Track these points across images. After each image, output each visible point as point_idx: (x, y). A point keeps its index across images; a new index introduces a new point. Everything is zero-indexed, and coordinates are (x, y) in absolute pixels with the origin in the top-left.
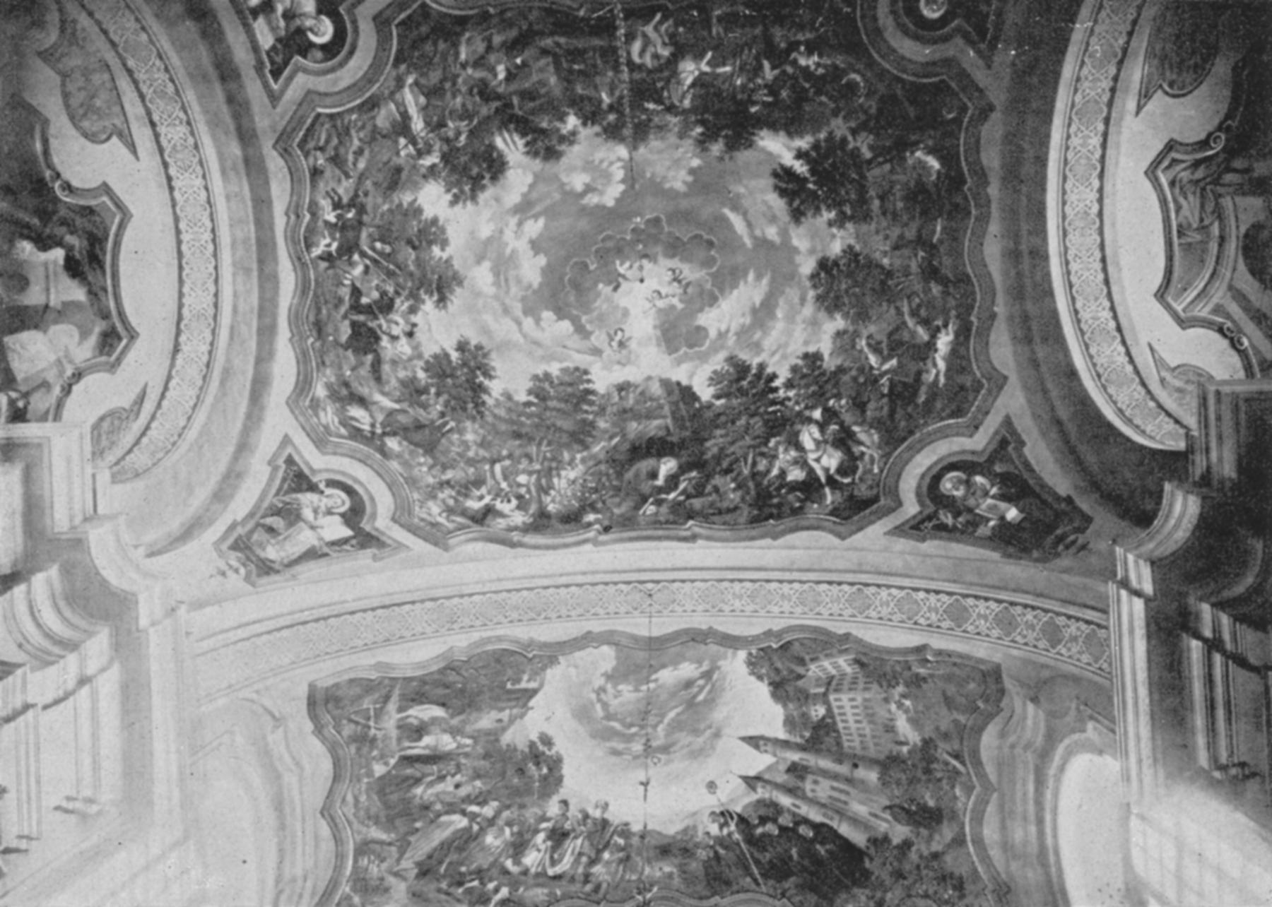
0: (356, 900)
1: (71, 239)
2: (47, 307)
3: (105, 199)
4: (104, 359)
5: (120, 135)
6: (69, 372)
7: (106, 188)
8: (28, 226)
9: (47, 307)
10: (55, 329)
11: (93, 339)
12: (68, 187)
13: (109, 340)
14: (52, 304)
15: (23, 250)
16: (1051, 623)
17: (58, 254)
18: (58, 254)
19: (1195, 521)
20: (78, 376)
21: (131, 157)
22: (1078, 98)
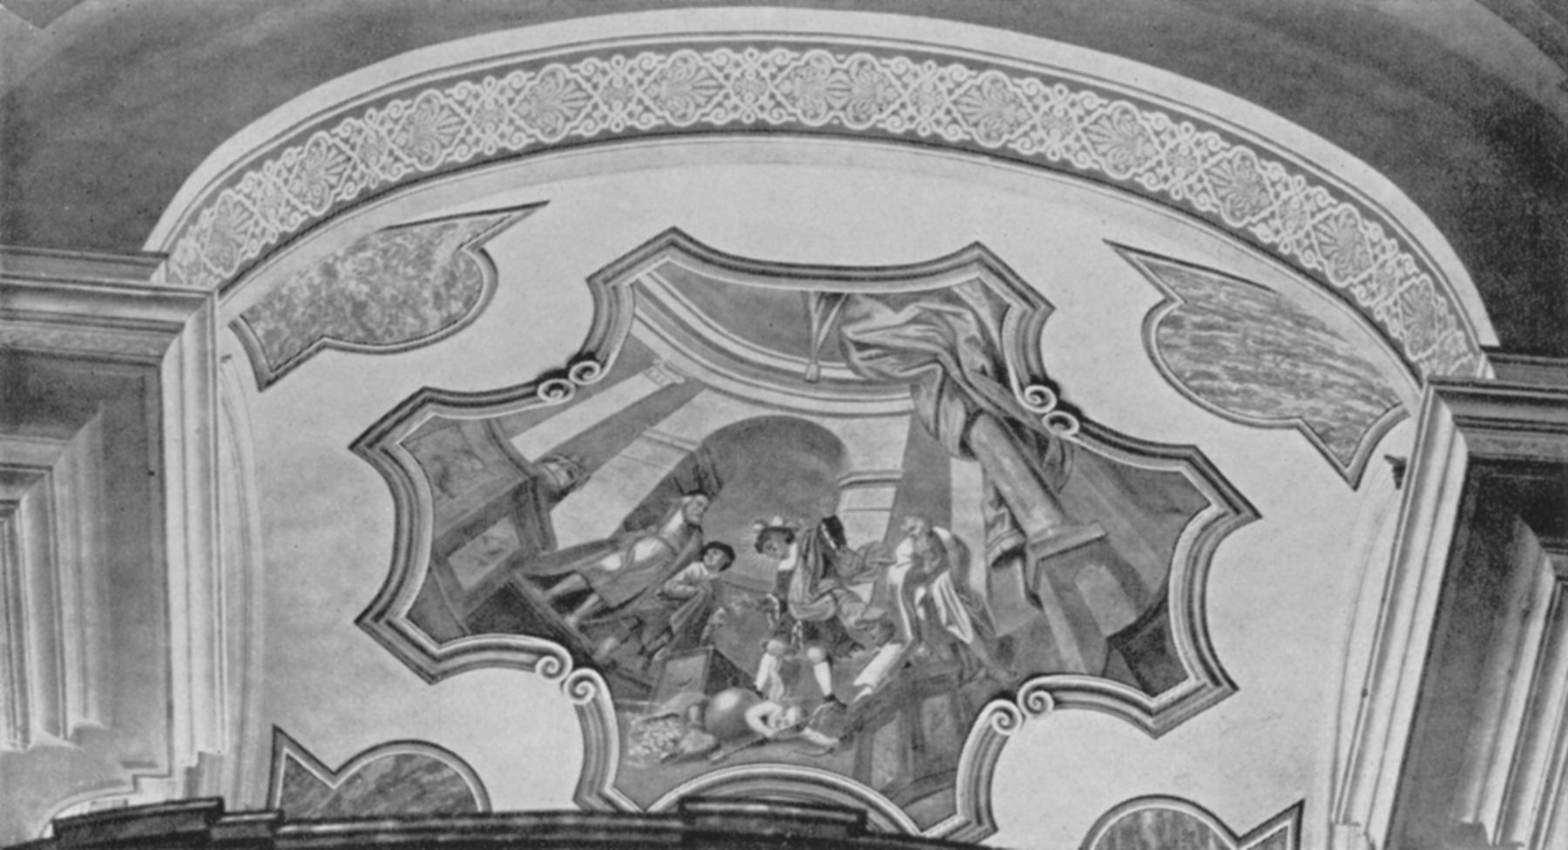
21: (540, 212)
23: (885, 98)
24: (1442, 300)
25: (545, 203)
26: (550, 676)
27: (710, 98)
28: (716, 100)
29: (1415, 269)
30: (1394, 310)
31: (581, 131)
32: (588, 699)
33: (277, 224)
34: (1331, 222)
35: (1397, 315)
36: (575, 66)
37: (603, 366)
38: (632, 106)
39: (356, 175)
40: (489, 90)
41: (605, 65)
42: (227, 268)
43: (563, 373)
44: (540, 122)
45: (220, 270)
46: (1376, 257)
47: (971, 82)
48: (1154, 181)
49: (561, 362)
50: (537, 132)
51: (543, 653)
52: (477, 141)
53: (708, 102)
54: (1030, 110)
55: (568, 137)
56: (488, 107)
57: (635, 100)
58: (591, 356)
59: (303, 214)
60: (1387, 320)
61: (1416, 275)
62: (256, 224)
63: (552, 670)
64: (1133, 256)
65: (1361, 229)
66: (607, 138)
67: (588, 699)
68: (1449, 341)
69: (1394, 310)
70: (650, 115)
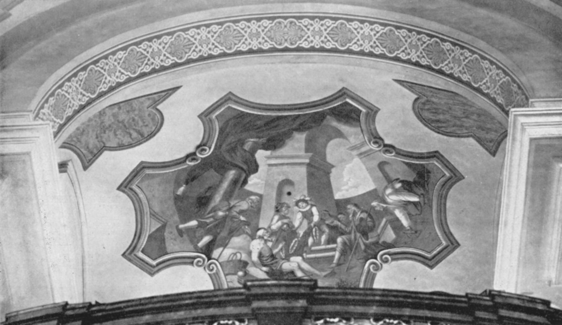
0: (269, 324)
1: (247, 146)
2: (309, 165)
3: (214, 116)
4: (362, 118)
5: (156, 103)
6: (374, 147)
7: (205, 116)
8: (235, 182)
9: (309, 165)
10: (330, 159)
11: (344, 128)
12: (201, 147)
13: (347, 114)
14: (307, 161)
15: (256, 184)
16: (509, 84)
17: (261, 155)
18: (261, 155)
19: (464, 315)
20: (377, 139)
21: (179, 91)
22: (447, 46)
23: (301, 35)
24: (515, 85)
25: (178, 88)
26: (200, 266)
27: (240, 41)
28: (242, 41)
29: (503, 75)
30: (497, 92)
31: (241, 49)
32: (214, 271)
33: (78, 101)
34: (471, 62)
35: (499, 94)
36: (187, 33)
37: (210, 148)
38: (210, 46)
39: (107, 81)
40: (155, 44)
41: (199, 31)
42: (62, 119)
43: (194, 154)
44: (129, 69)
45: (58, 121)
46: (488, 73)
47: (239, 45)
48: (404, 55)
49: (191, 150)
50: (224, 48)
51: (194, 258)
52: (250, 44)
53: (239, 42)
54: (356, 34)
55: (236, 51)
56: (155, 51)
57: (211, 44)
58: (205, 145)
59: (87, 97)
60: (495, 96)
61: (504, 78)
62: (70, 102)
63: (200, 264)
64: (405, 84)
65: (481, 64)
66: (251, 52)
67: (214, 271)
68: (520, 100)
69: (497, 92)
70: (169, 60)
